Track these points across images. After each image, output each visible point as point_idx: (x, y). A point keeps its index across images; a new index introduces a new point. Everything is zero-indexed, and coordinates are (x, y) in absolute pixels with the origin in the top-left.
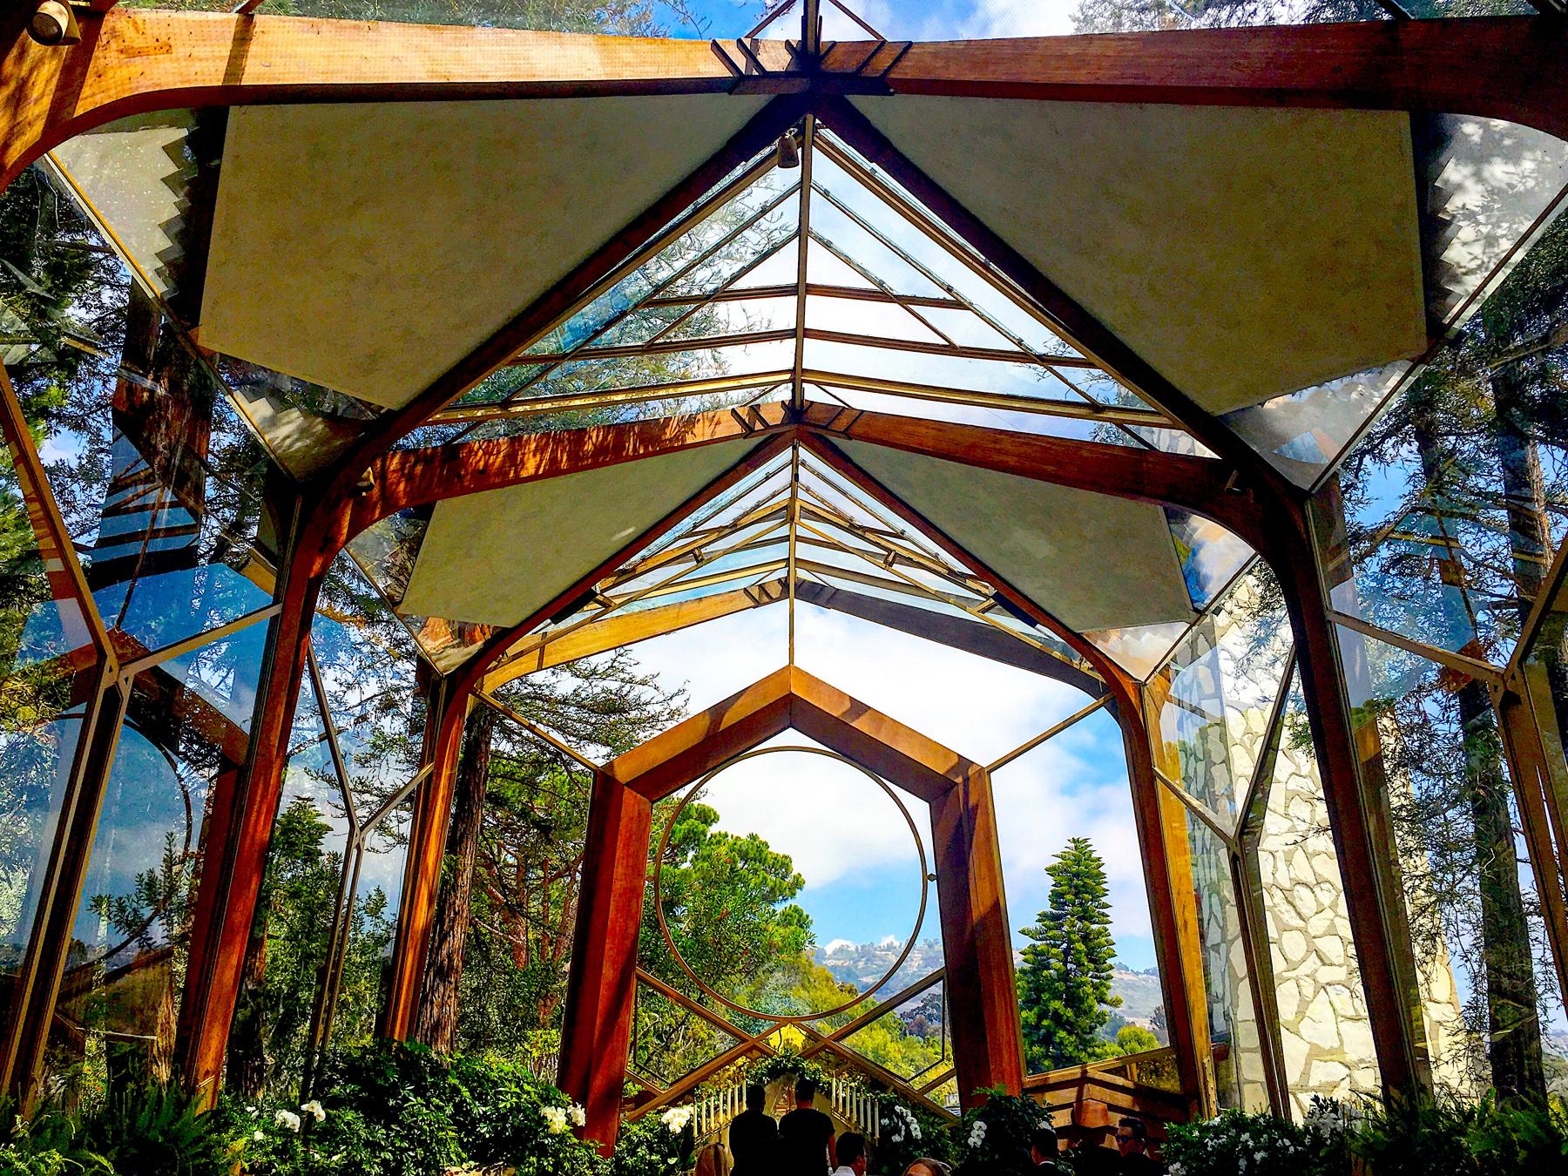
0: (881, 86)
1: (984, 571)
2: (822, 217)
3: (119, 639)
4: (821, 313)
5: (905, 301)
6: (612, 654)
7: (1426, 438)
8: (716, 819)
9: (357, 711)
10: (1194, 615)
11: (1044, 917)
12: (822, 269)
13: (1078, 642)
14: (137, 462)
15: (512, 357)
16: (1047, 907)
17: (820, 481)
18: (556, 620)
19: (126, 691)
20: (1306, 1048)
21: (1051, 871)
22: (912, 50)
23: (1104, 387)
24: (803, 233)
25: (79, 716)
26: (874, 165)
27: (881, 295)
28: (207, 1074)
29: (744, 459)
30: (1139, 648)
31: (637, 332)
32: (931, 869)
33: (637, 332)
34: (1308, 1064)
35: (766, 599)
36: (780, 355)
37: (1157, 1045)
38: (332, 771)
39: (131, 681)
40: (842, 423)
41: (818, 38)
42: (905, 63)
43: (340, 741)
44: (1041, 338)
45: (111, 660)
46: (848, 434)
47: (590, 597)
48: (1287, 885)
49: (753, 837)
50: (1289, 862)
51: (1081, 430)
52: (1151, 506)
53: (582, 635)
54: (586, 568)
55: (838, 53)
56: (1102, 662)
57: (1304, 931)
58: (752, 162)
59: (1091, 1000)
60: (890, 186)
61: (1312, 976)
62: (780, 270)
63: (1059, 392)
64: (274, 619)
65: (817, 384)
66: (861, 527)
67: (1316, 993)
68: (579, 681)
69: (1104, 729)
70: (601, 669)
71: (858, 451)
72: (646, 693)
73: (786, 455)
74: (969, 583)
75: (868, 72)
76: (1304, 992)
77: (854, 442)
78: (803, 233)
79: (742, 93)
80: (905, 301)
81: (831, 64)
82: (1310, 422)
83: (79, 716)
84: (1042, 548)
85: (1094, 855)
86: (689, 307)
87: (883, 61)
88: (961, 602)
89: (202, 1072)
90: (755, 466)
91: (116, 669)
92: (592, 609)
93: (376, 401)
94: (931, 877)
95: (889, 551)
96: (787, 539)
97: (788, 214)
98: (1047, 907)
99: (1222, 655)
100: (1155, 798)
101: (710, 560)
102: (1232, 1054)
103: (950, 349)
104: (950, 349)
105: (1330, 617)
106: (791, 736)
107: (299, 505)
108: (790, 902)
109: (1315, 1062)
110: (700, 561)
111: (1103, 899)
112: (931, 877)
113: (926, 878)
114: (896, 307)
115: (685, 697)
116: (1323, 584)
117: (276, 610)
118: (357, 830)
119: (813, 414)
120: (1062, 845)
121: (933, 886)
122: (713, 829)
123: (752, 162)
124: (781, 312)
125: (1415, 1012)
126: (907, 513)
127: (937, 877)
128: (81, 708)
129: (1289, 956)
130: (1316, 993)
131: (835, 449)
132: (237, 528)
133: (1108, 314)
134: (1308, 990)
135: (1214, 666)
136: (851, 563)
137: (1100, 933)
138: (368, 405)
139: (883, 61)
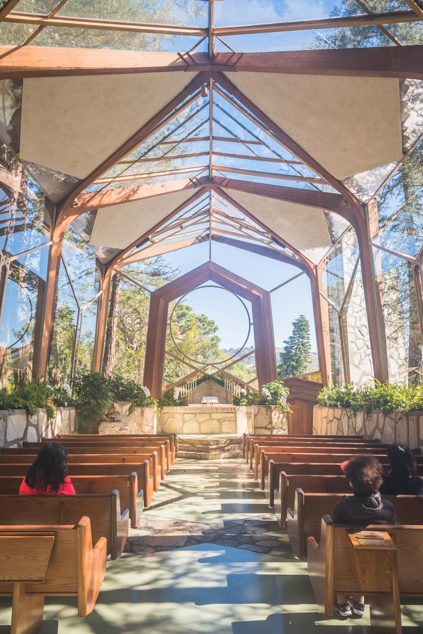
0: (233, 68)
1: (269, 231)
2: (217, 114)
4: (218, 147)
5: (243, 142)
6: (156, 258)
7: (406, 188)
8: (192, 309)
9: (79, 275)
10: (332, 244)
11: (290, 337)
12: (219, 132)
13: (296, 252)
14: (5, 197)
15: (119, 161)
16: (292, 335)
17: (217, 201)
18: (138, 246)
19: (8, 267)
20: (361, 372)
21: (294, 324)
22: (244, 56)
23: (307, 171)
24: (211, 119)
26: (232, 96)
27: (236, 140)
28: (42, 377)
29: (194, 195)
30: (316, 255)
31: (158, 152)
32: (252, 322)
33: (158, 152)
34: (361, 376)
36: (204, 161)
38: (72, 293)
40: (225, 183)
41: (213, 52)
42: (241, 60)
43: (74, 285)
44: (288, 155)
46: (226, 186)
47: (147, 239)
48: (359, 326)
49: (203, 315)
50: (360, 319)
51: (301, 185)
52: (319, 210)
53: (148, 251)
54: (146, 231)
55: (219, 57)
57: (363, 340)
58: (194, 94)
59: (303, 362)
61: (365, 352)
62: (204, 132)
63: (292, 173)
65: (217, 170)
66: (232, 217)
67: (365, 357)
68: (146, 266)
69: (305, 279)
70: (152, 262)
71: (229, 191)
72: (167, 270)
73: (207, 194)
74: (265, 234)
75: (229, 63)
76: (362, 356)
77: (229, 189)
78: (211, 119)
79: (189, 71)
80: (243, 142)
81: (219, 58)
82: (367, 182)
85: (306, 320)
87: (234, 59)
88: (261, 241)
89: (40, 377)
90: (198, 197)
91: (4, 260)
92: (148, 243)
93: (78, 177)
94: (252, 324)
95: (241, 225)
96: (209, 221)
97: (204, 114)
98: (292, 335)
99: (344, 257)
100: (319, 300)
101: (185, 228)
102: (340, 374)
103: (258, 158)
104: (258, 158)
106: (210, 282)
107: (386, 455)
108: (214, 334)
109: (364, 376)
111: (308, 333)
112: (252, 324)
113: (250, 324)
114: (241, 144)
115: (179, 270)
119: (216, 180)
120: (298, 317)
121: (252, 326)
122: (191, 313)
123: (194, 94)
124: (204, 146)
126: (245, 212)
127: (254, 324)
129: (358, 347)
130: (365, 357)
131: (223, 192)
132: (37, 218)
133: (305, 146)
134: (363, 355)
135: (342, 259)
136: (229, 229)
137: (307, 343)
138: (76, 178)
139: (234, 59)
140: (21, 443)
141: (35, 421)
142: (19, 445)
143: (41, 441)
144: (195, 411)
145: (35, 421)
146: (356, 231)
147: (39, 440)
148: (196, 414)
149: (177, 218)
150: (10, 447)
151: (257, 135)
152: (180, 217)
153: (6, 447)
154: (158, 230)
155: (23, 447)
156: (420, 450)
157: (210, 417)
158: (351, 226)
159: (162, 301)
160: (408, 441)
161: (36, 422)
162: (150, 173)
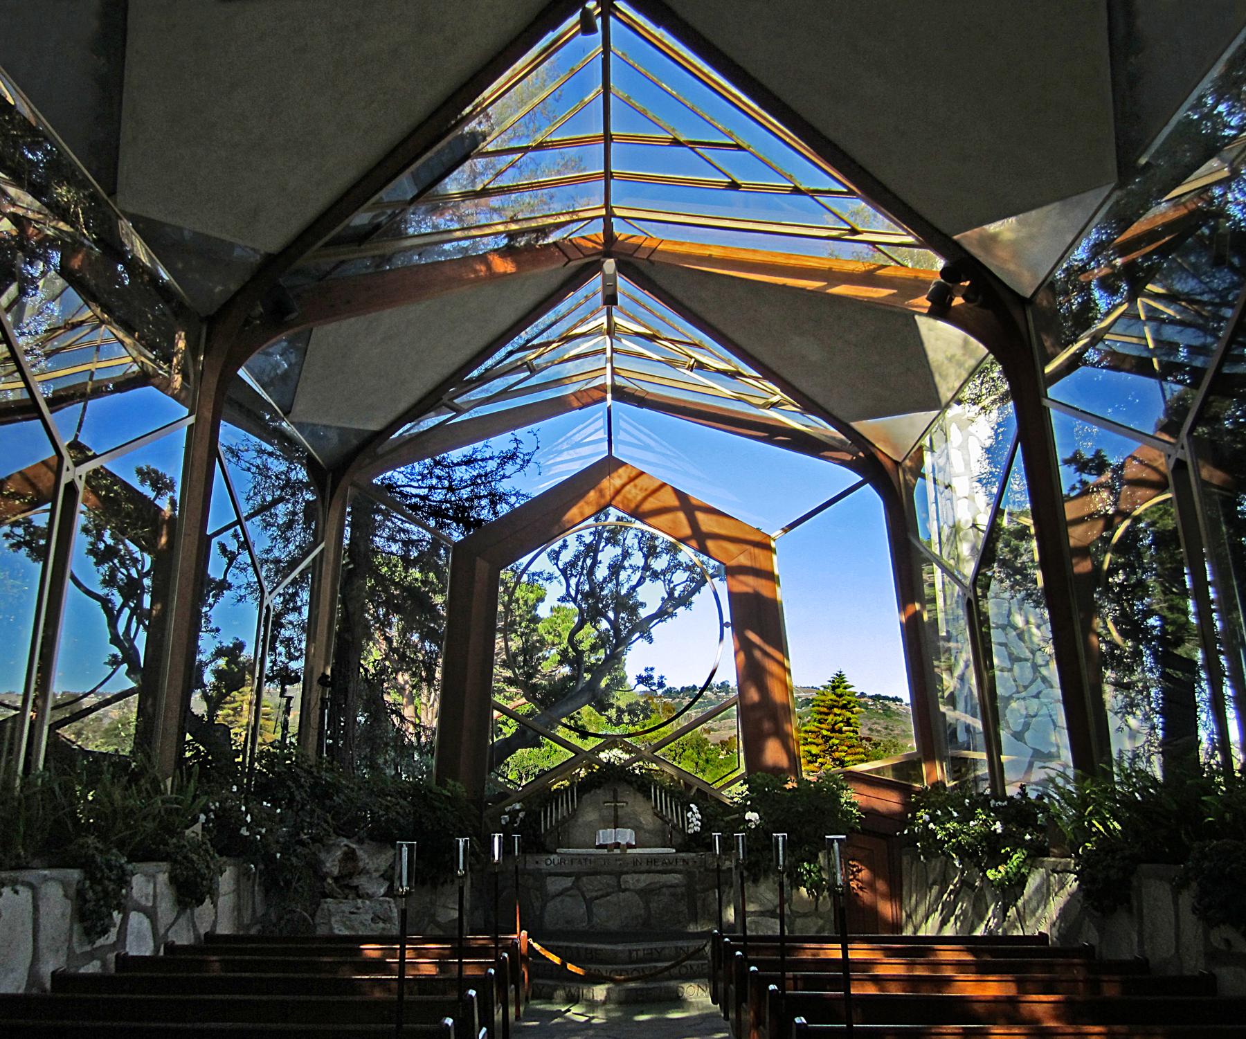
3: (75, 446)
19: (81, 485)
25: (45, 511)
30: (891, 432)
32: (727, 618)
35: (579, 395)
37: (163, 878)
39: (84, 478)
45: (68, 462)
56: (859, 440)
60: (685, 55)
64: (190, 427)
83: (45, 511)
84: (814, 353)
86: (516, 157)
94: (727, 625)
105: (1046, 402)
110: (533, 371)
112: (727, 625)
116: (1042, 386)
117: (192, 420)
118: (266, 594)
125: (432, 413)
128: (48, 506)
140: (112, 957)
141: (147, 899)
142: (104, 965)
143: (162, 953)
144: (576, 867)
145: (147, 895)
146: (1008, 373)
147: (157, 949)
148: (578, 876)
149: (522, 342)
150: (82, 971)
151: (606, 443)
152: (528, 341)
153: (72, 970)
154: (475, 373)
155: (117, 971)
156: (1213, 977)
158: (991, 356)
159: (482, 565)
160: (1177, 951)
161: (151, 898)
162: (469, 228)
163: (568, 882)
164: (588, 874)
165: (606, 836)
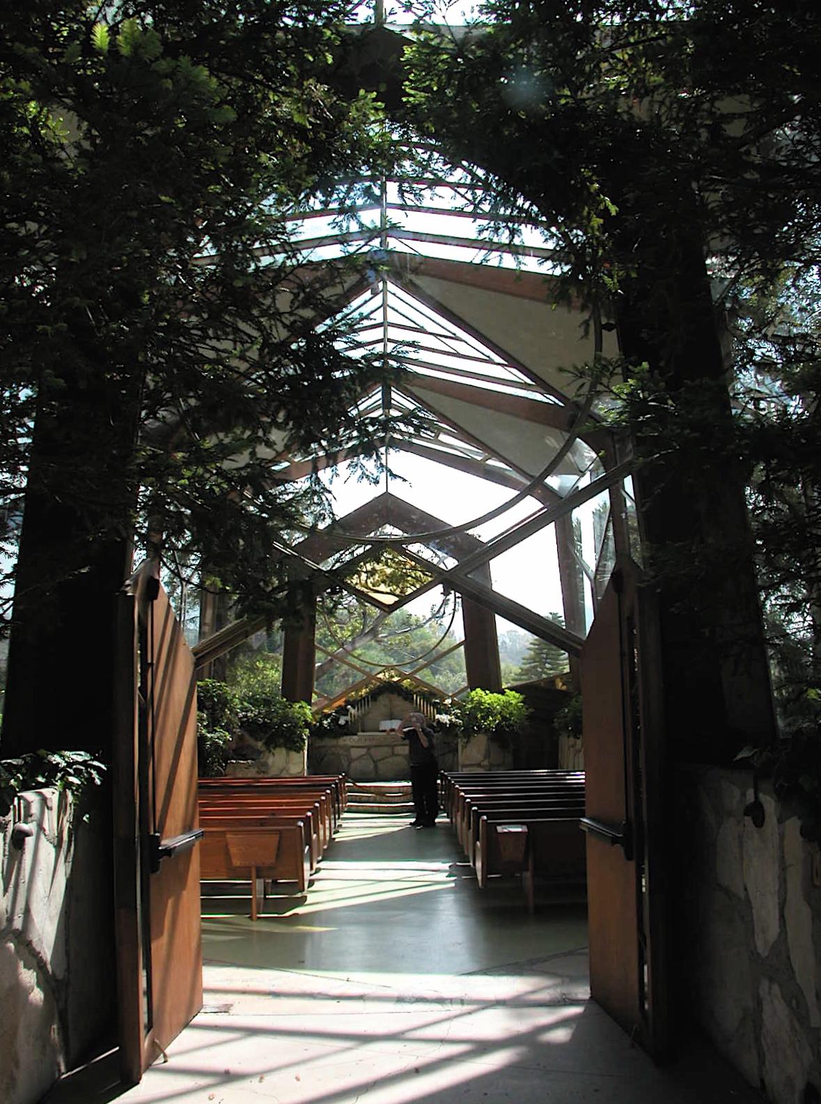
2: (391, 300)
4: (394, 333)
12: (393, 317)
44: (498, 359)
103: (457, 355)
124: (377, 334)
144: (367, 743)
148: (369, 748)
157: (393, 753)
163: (364, 751)
164: (375, 746)
165: (386, 725)
